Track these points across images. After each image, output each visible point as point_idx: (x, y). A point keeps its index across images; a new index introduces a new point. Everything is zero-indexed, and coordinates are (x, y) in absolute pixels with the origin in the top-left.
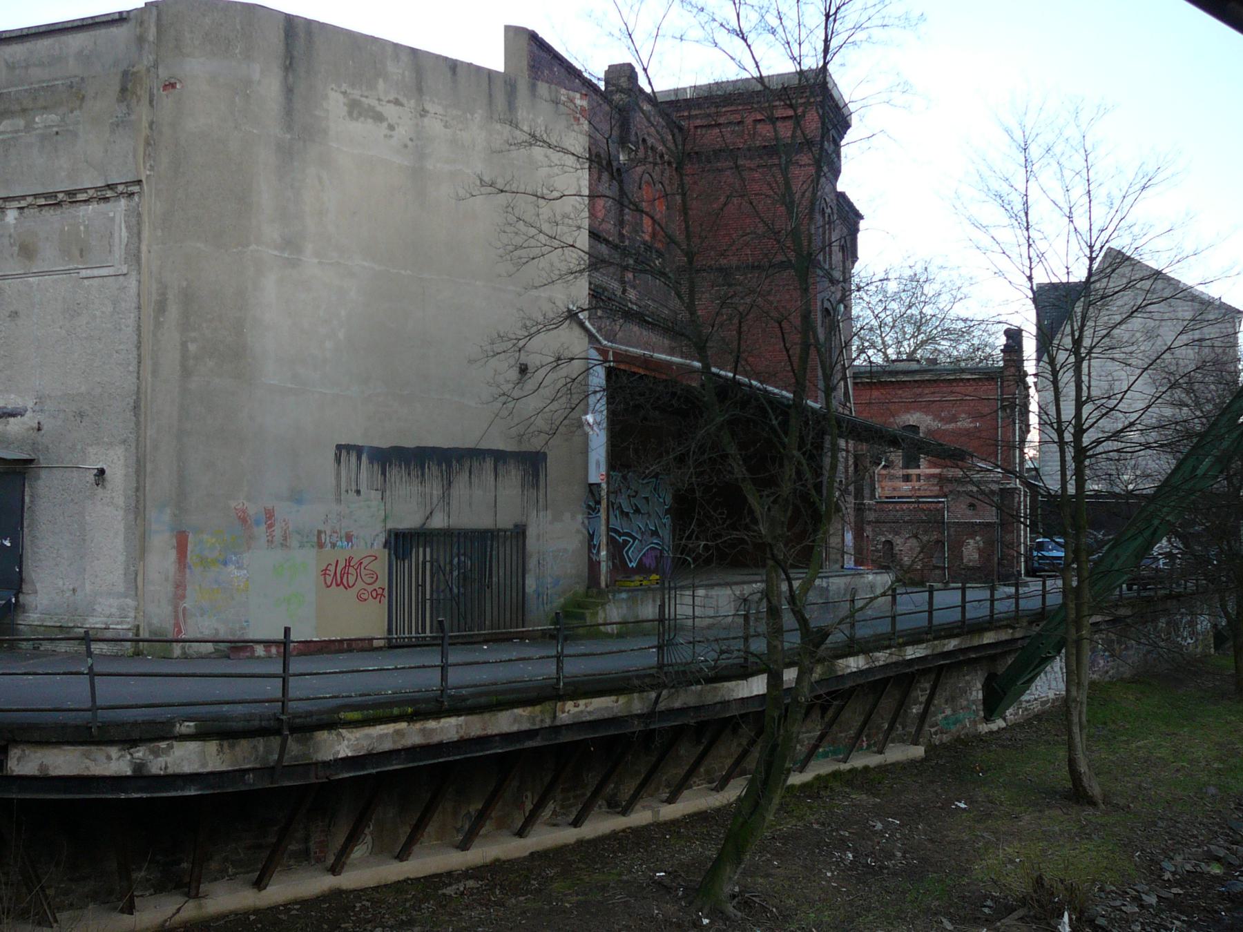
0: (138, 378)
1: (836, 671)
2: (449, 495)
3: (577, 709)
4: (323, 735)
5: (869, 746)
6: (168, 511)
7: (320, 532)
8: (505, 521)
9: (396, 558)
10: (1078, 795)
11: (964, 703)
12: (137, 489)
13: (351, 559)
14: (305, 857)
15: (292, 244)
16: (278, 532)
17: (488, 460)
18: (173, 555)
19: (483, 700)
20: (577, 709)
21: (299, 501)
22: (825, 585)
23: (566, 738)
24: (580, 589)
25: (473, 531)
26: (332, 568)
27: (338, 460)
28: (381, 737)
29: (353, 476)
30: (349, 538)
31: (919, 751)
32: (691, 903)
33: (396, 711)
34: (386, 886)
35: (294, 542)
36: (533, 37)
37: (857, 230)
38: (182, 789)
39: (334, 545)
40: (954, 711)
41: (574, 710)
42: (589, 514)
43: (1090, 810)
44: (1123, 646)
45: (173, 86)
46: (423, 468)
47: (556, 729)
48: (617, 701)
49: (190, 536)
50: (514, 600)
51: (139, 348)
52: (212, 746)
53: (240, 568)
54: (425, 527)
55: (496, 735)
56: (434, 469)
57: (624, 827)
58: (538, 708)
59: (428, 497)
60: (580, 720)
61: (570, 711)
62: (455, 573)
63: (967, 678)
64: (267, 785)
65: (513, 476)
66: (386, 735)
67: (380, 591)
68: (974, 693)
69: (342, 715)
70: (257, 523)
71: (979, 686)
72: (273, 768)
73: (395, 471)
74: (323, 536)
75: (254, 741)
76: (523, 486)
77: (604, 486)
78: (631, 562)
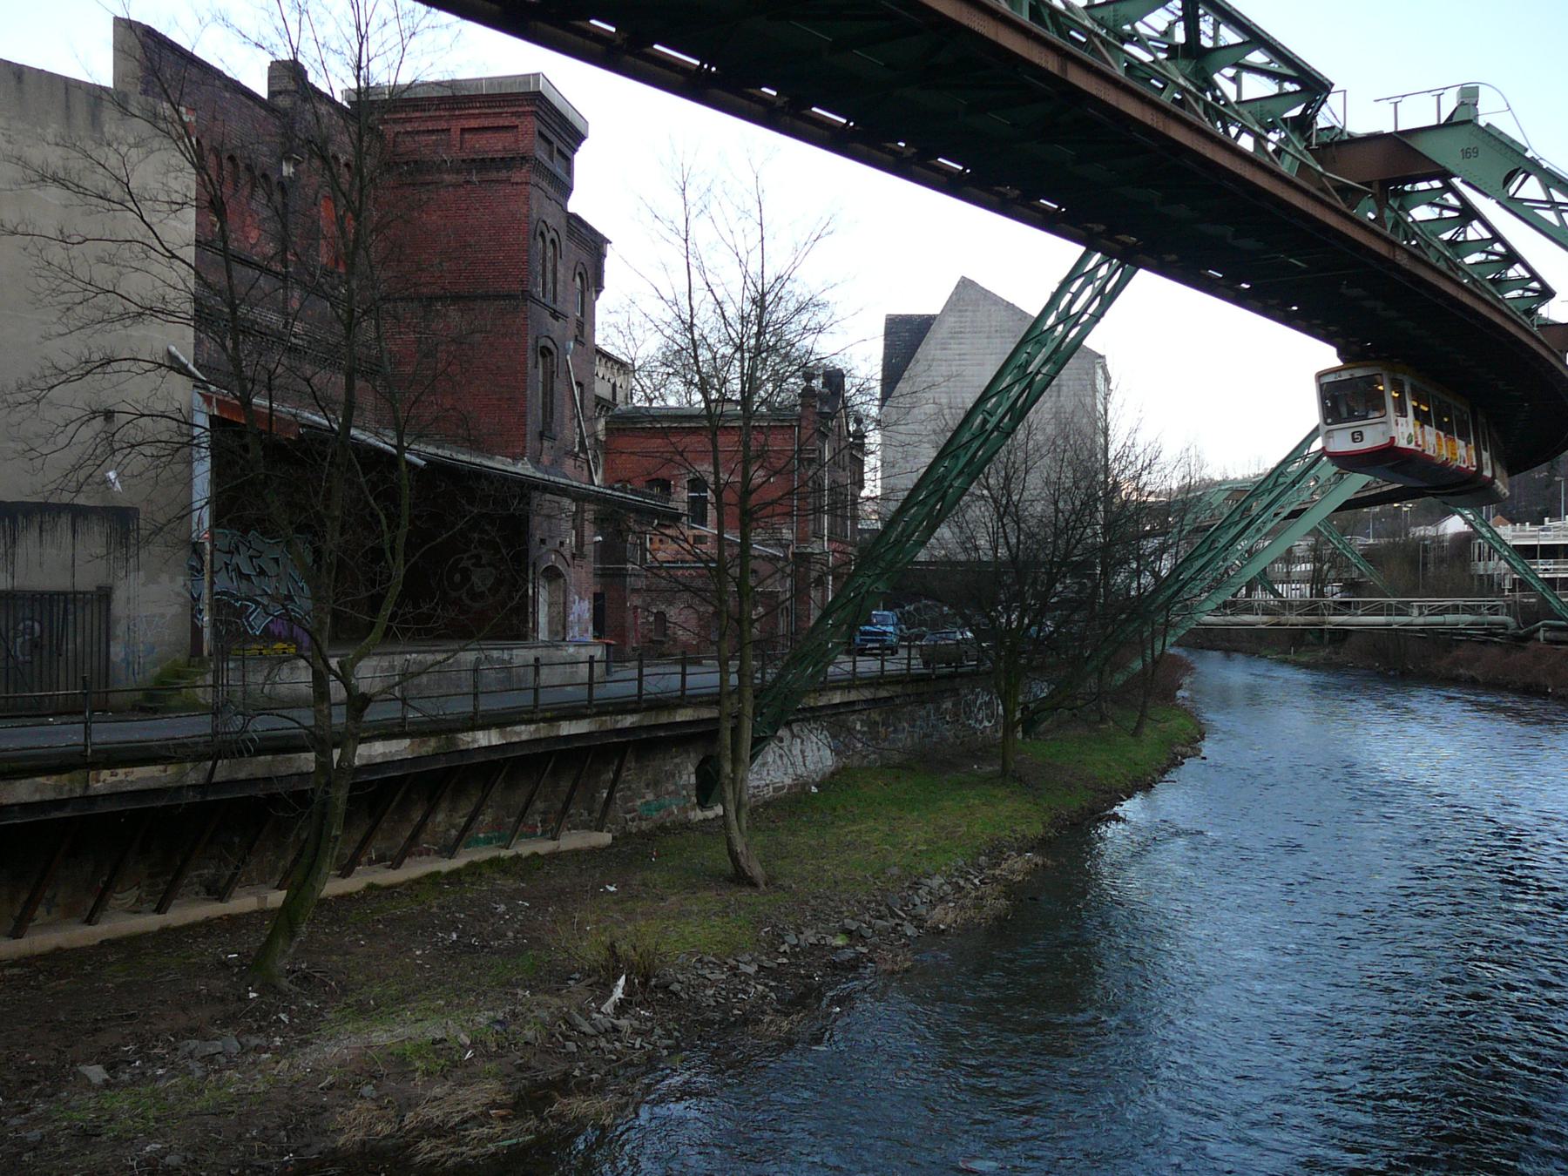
2: (13, 555)
3: (114, 779)
8: (86, 581)
10: (741, 878)
11: (672, 788)
22: (506, 657)
24: (181, 657)
25: (42, 594)
31: (605, 838)
36: (149, 32)
40: (658, 797)
41: (111, 780)
42: (192, 575)
43: (747, 891)
44: (891, 729)
47: (92, 800)
48: (165, 771)
55: (13, 805)
57: (220, 913)
58: (65, 777)
60: (119, 790)
61: (106, 780)
62: (19, 640)
63: (677, 760)
65: (94, 541)
68: (685, 777)
71: (692, 769)
76: (108, 544)
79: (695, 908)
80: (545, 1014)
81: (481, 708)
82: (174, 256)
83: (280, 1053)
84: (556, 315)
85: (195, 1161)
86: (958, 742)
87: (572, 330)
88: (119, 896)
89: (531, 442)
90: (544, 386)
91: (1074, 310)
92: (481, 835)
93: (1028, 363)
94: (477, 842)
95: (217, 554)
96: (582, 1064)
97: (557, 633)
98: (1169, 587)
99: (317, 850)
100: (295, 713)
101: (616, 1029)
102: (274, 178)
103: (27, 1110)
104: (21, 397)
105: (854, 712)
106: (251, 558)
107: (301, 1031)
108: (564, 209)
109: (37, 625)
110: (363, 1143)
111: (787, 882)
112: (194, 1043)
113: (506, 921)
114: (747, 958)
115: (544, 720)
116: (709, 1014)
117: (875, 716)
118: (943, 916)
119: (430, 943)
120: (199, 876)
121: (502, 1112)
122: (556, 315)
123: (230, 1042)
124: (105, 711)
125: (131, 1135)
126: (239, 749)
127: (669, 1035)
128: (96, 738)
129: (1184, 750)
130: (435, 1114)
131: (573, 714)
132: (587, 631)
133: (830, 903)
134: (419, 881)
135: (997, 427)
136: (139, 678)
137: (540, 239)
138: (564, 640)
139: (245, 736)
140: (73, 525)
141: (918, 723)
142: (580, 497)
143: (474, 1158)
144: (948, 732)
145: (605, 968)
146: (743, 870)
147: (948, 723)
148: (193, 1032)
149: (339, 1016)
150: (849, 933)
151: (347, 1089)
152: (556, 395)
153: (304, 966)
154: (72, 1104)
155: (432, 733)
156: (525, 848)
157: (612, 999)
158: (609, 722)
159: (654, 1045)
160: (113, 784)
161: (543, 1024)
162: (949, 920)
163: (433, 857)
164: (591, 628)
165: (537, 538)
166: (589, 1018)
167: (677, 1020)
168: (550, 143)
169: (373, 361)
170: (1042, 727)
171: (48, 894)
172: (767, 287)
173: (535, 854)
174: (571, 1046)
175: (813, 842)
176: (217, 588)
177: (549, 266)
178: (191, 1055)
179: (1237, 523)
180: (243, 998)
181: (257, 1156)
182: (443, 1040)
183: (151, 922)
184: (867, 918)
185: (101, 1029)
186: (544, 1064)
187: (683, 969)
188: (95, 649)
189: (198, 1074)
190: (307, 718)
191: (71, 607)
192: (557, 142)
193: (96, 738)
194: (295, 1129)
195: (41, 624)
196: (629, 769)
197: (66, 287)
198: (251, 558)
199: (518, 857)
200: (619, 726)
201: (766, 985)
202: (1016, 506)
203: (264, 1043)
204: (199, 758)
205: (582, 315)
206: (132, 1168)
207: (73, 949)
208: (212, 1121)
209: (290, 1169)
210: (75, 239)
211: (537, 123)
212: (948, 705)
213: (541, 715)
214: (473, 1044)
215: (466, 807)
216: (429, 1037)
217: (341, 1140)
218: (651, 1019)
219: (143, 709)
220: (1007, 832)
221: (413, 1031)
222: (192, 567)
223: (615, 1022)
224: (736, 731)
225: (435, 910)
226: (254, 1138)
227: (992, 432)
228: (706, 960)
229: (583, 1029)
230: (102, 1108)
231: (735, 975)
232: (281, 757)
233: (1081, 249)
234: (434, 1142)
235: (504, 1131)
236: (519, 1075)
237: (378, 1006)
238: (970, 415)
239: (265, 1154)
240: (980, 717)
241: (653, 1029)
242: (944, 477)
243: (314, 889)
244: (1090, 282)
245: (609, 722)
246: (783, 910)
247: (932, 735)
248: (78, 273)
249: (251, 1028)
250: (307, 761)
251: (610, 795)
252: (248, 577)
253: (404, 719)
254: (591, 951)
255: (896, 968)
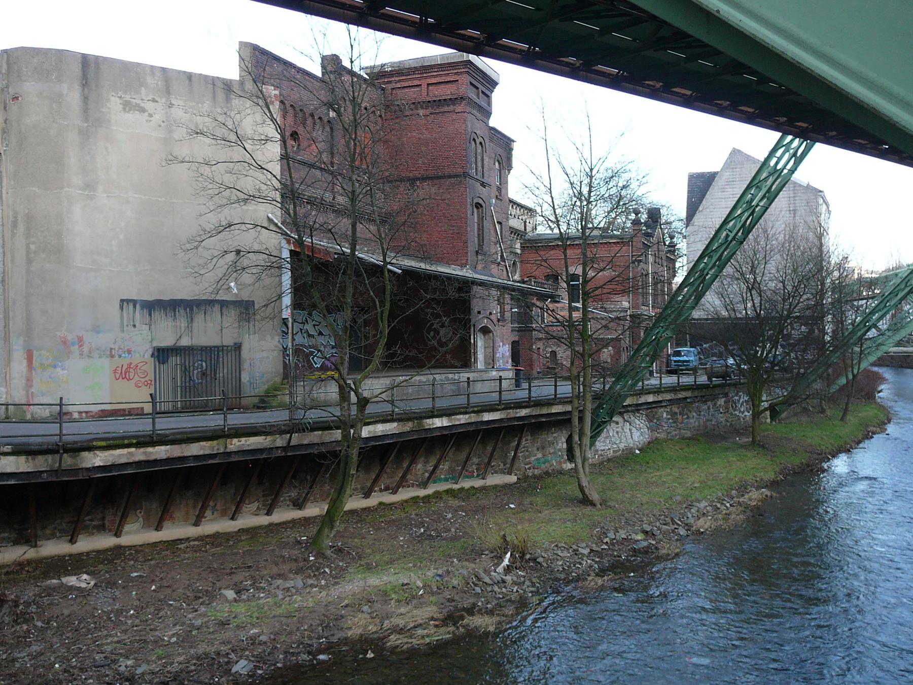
0: (4, 264)
1: (423, 426)
3: (240, 443)
4: (85, 454)
5: (478, 476)
6: (22, 338)
7: (111, 349)
8: (228, 339)
9: (159, 363)
10: (586, 501)
11: (552, 451)
12: (5, 327)
13: (131, 364)
14: (102, 528)
15: (90, 186)
16: (86, 349)
17: (216, 305)
18: (25, 363)
19: (178, 437)
20: (240, 443)
21: (98, 332)
22: (456, 377)
23: (234, 459)
24: (278, 379)
25: (206, 347)
26: (119, 369)
27: (122, 308)
28: (120, 455)
29: (131, 318)
30: (129, 352)
31: (513, 479)
32: (306, 549)
33: (126, 442)
34: (148, 544)
35: (96, 355)
37: (511, 149)
38: (7, 481)
39: (120, 356)
40: (544, 455)
41: (238, 444)
43: (589, 508)
45: (17, 98)
46: (175, 311)
49: (35, 352)
50: (234, 387)
51: (3, 248)
52: (22, 459)
53: (63, 369)
54: (177, 345)
56: (182, 312)
57: (300, 516)
58: (215, 442)
59: (178, 329)
61: (236, 444)
62: (196, 372)
64: (55, 479)
65: (231, 317)
66: (123, 455)
67: (149, 382)
69: (95, 443)
70: (73, 344)
71: (564, 440)
72: (57, 470)
73: (157, 313)
74: (113, 351)
75: (46, 456)
77: (290, 319)
78: (316, 364)
79: (558, 517)
80: (465, 573)
81: (437, 406)
82: (262, 168)
83: (322, 588)
84: (483, 185)
85: (275, 639)
86: (728, 424)
87: (494, 192)
88: (248, 506)
89: (471, 256)
90: (479, 225)
91: (778, 167)
92: (442, 477)
93: (752, 200)
94: (440, 480)
95: (295, 324)
96: (483, 599)
97: (489, 364)
98: (860, 330)
99: (344, 479)
100: (330, 409)
101: (504, 581)
102: (325, 119)
103: (196, 611)
104: (189, 246)
105: (662, 406)
106: (314, 325)
107: (336, 578)
108: (487, 125)
109: (204, 364)
110: (361, 635)
111: (612, 504)
112: (279, 582)
113: (451, 523)
114: (584, 545)
115: (474, 412)
116: (558, 575)
117: (675, 409)
118: (704, 524)
119: (409, 534)
120: (289, 496)
121: (437, 623)
122: (483, 185)
123: (298, 581)
124: (239, 409)
125: (244, 625)
126: (302, 428)
127: (533, 585)
128: (229, 422)
129: (874, 429)
130: (401, 622)
131: (491, 409)
132: (508, 362)
133: (637, 516)
134: (406, 501)
135: (734, 238)
136: (256, 391)
137: (473, 143)
138: (493, 367)
139: (306, 421)
140: (221, 311)
141: (702, 413)
142: (503, 288)
143: (418, 645)
144: (722, 418)
145: (500, 548)
146: (587, 497)
147: (721, 413)
148: (280, 576)
149: (356, 570)
150: (646, 533)
151: (355, 607)
152: (485, 230)
153: (339, 544)
154: (218, 609)
155: (409, 420)
156: (467, 484)
157: (502, 565)
158: (513, 413)
159: (525, 591)
160: (239, 446)
161: (464, 577)
162: (706, 526)
163: (415, 488)
164: (510, 361)
165: (476, 310)
166: (489, 575)
167: (539, 578)
168: (477, 88)
169: (383, 215)
170: (784, 415)
171: (211, 503)
172: (594, 163)
173: (473, 488)
174: (478, 590)
175: (631, 481)
176: (296, 342)
177: (479, 158)
178: (278, 587)
179: (903, 290)
180: (306, 560)
181: (306, 639)
182: (407, 584)
183: (264, 520)
184: (658, 524)
185: (234, 573)
186: (462, 598)
187: (546, 550)
188: (234, 375)
189: (281, 597)
190: (337, 411)
191: (221, 353)
192: (481, 88)
193: (229, 422)
194: (326, 627)
195: (206, 362)
196: (526, 440)
197: (210, 186)
198: (314, 325)
199: (463, 489)
200: (518, 415)
201: (593, 560)
202: (759, 284)
203: (316, 583)
204: (282, 432)
205: (500, 184)
206: (243, 641)
207: (224, 533)
208: (284, 620)
209: (323, 646)
210: (214, 163)
211: (469, 78)
212: (721, 402)
213: (471, 410)
214: (424, 587)
215: (433, 461)
216: (400, 582)
217: (350, 633)
218: (524, 577)
219: (258, 408)
220: (751, 477)
221: (391, 578)
222: (283, 332)
223: (504, 577)
224: (581, 419)
225: (413, 516)
226: (305, 630)
227: (731, 241)
228: (559, 546)
229: (485, 581)
230: (231, 611)
231: (576, 554)
232: (326, 432)
233: (780, 134)
234: (398, 636)
235: (435, 632)
236: (448, 604)
237: (377, 566)
238: (718, 232)
239: (310, 638)
240: (742, 410)
241: (524, 582)
242: (704, 269)
243: (342, 502)
244: (787, 150)
245: (513, 413)
246: (608, 519)
247: (711, 420)
248: (216, 179)
249: (310, 575)
250: (337, 435)
251: (515, 454)
252: (313, 336)
253: (393, 411)
254: (494, 540)
255: (670, 552)
